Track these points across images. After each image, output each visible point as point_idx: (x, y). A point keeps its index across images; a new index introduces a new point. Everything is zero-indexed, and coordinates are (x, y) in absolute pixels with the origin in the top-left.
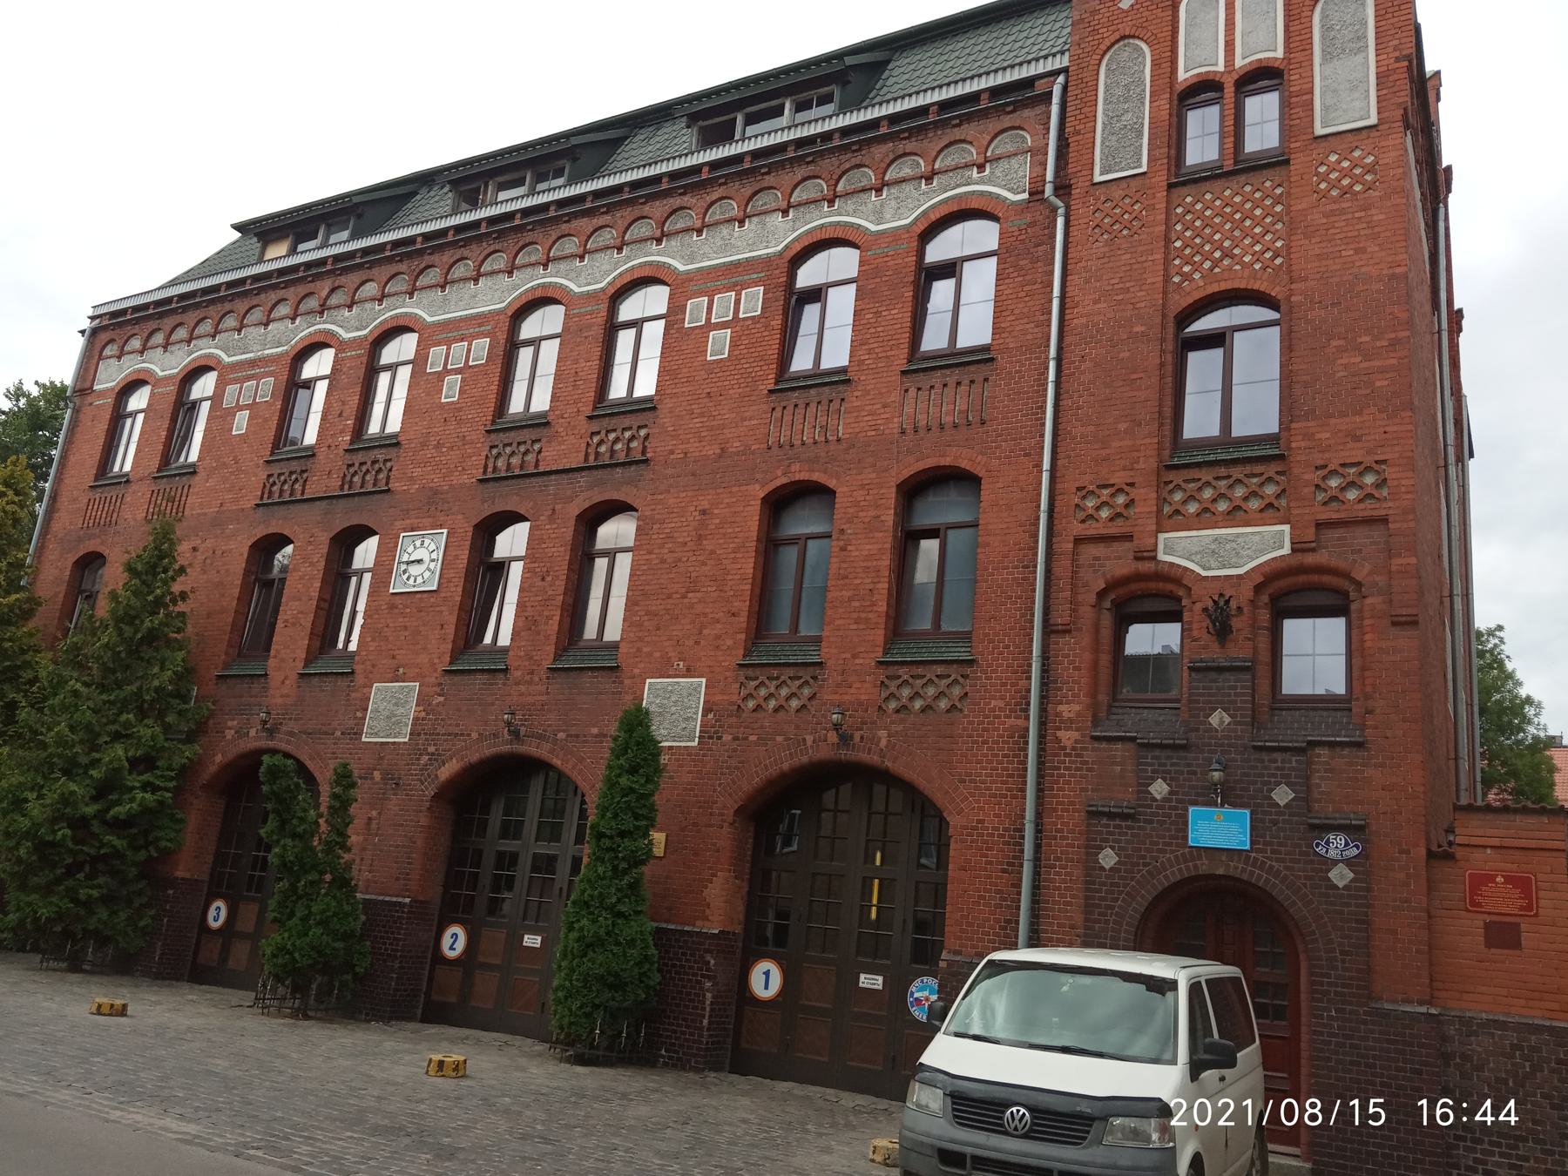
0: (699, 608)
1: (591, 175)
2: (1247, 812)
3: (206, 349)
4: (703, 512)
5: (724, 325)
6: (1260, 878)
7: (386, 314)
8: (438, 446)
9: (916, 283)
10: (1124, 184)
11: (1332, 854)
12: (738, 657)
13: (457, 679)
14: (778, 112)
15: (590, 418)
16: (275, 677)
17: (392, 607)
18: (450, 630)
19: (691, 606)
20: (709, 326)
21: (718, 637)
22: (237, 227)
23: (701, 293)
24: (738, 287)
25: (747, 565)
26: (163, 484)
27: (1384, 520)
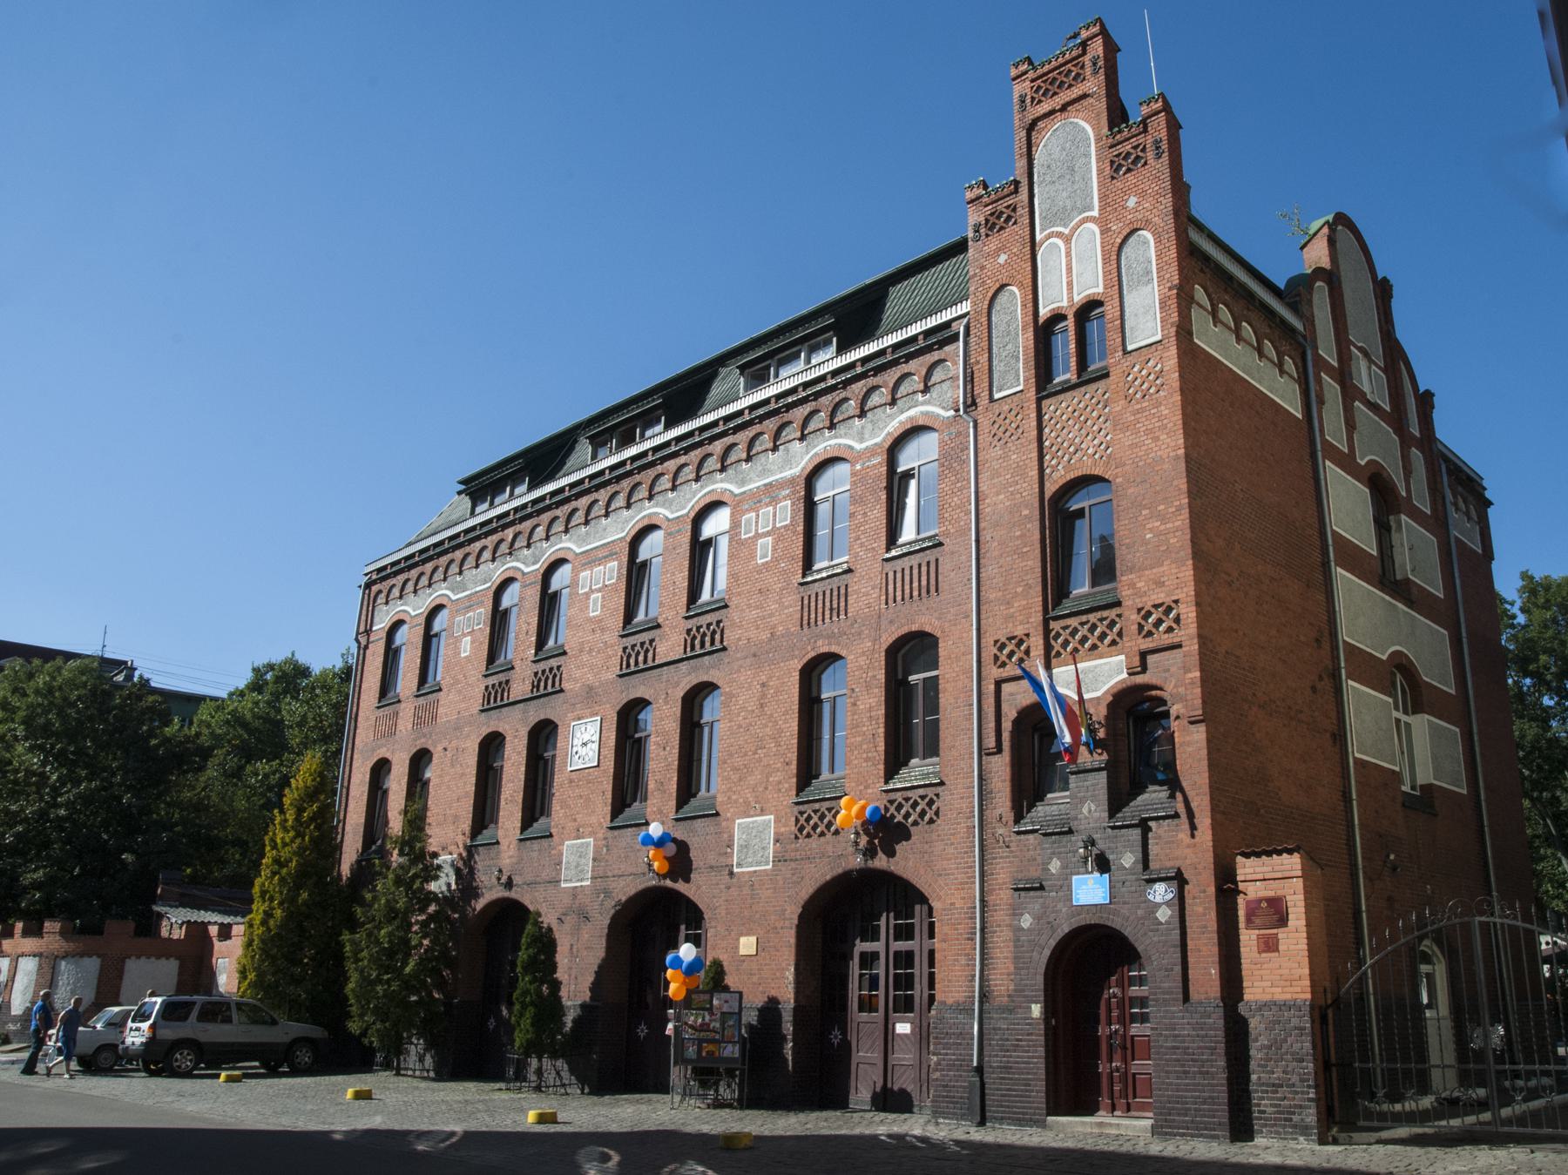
0: (765, 762)
1: (551, 477)
2: (1074, 878)
3: (720, 485)
4: (763, 685)
5: (768, 534)
6: (1116, 923)
7: (895, 422)
8: (591, 650)
9: (889, 489)
10: (1009, 400)
11: (1158, 899)
12: (672, 815)
13: (616, 833)
14: (796, 356)
15: (687, 618)
16: (504, 843)
17: (571, 781)
18: (609, 795)
19: (760, 760)
20: (758, 536)
21: (780, 782)
22: (461, 482)
23: (748, 511)
24: (774, 501)
25: (793, 725)
26: (421, 701)
27: (1179, 646)
